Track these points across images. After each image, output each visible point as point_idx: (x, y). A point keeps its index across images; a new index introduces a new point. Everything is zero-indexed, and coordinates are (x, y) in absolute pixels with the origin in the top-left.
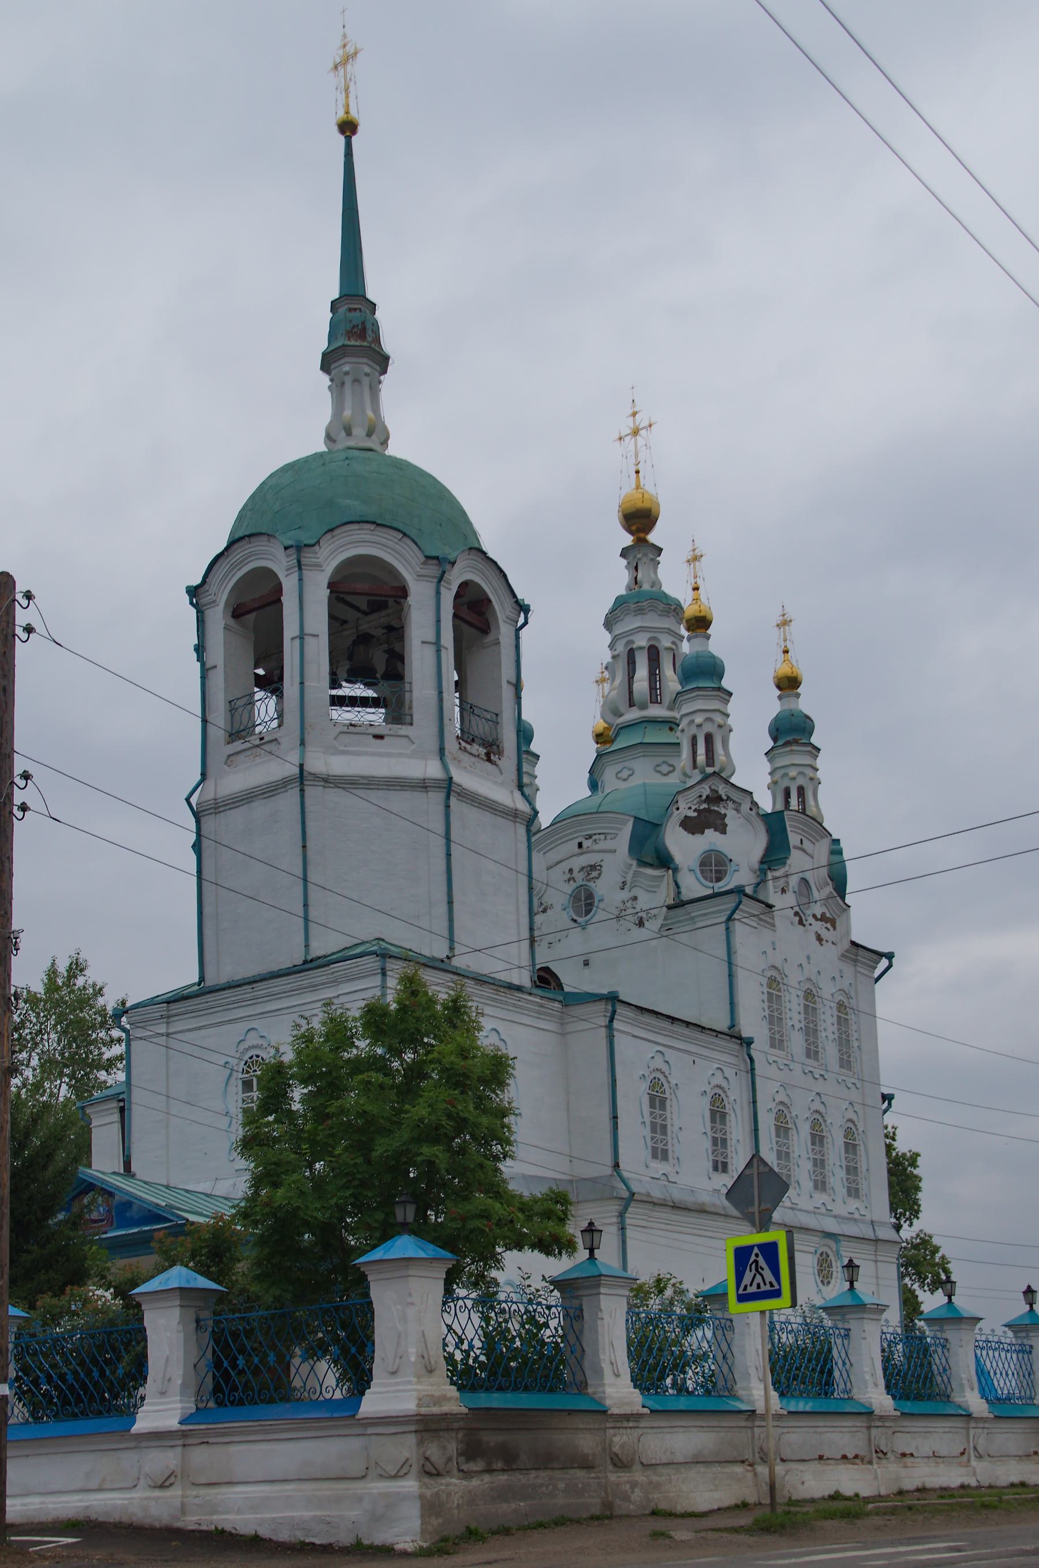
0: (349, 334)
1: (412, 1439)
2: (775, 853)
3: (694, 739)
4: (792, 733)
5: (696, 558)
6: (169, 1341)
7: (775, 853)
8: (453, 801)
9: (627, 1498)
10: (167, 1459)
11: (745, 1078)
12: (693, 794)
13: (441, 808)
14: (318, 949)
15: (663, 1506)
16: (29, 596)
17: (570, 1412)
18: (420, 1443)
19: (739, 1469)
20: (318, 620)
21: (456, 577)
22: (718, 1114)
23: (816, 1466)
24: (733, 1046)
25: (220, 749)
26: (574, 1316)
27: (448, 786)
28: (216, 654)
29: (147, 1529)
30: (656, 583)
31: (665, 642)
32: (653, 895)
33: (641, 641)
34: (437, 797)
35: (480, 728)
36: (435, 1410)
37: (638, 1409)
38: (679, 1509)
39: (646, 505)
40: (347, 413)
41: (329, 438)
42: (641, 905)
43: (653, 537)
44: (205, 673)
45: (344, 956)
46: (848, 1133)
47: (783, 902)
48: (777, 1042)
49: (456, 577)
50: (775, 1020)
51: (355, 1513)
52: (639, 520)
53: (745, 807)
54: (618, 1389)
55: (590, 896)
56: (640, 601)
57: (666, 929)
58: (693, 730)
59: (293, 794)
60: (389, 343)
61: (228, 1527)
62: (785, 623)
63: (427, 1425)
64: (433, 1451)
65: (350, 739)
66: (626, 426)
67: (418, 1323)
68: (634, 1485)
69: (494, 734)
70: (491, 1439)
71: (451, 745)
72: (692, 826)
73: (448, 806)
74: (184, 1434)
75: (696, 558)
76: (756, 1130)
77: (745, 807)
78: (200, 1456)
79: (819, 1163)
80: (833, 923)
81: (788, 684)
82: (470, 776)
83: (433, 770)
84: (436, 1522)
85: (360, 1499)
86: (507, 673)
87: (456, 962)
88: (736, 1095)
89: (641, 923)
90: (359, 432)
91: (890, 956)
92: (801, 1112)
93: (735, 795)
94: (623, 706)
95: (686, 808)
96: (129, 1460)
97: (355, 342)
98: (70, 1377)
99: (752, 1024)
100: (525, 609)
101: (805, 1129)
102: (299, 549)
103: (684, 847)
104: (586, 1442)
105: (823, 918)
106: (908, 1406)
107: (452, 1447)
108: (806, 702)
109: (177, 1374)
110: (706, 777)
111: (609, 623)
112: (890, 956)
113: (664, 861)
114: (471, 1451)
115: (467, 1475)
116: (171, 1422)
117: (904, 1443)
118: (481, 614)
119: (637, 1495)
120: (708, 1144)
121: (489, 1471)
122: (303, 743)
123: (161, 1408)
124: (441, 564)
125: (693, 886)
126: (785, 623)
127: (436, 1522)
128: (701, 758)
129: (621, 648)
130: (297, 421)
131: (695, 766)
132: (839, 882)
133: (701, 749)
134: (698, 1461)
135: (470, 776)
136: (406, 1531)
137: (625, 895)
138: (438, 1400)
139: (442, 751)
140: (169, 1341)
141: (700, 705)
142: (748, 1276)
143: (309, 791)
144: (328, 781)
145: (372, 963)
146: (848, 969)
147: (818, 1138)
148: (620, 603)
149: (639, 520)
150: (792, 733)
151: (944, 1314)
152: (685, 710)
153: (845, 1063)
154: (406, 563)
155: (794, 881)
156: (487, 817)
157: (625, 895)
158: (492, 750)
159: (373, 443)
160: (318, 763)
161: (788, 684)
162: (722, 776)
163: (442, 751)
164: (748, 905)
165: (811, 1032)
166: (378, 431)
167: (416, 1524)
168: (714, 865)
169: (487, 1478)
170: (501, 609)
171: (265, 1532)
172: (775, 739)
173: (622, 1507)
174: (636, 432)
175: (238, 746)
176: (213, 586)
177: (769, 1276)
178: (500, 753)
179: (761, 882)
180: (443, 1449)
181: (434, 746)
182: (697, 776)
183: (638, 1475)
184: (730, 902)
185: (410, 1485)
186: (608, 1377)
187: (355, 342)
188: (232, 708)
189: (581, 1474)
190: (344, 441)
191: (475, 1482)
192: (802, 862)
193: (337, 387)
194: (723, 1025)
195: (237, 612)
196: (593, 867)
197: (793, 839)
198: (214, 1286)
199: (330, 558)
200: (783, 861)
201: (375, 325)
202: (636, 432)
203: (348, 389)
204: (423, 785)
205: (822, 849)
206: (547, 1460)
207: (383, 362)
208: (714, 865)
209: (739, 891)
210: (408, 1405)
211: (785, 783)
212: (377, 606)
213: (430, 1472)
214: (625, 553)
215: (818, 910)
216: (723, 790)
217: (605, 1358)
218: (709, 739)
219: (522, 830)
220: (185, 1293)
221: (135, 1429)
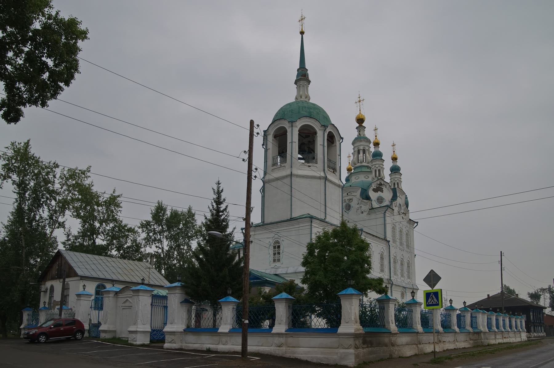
0: (302, 76)
1: (352, 339)
2: (394, 198)
3: (376, 170)
4: (395, 170)
5: (376, 129)
6: (281, 311)
7: (394, 198)
8: (327, 182)
9: (394, 354)
10: (282, 340)
11: (388, 250)
12: (375, 183)
13: (324, 184)
14: (294, 216)
15: (401, 355)
16: (258, 126)
17: (384, 333)
18: (355, 340)
19: (415, 346)
20: (296, 138)
21: (328, 130)
22: (382, 258)
23: (428, 345)
24: (385, 242)
25: (270, 168)
26: (382, 309)
27: (326, 178)
28: (270, 145)
29: (332, 366)
30: (364, 135)
31: (367, 148)
32: (365, 207)
33: (362, 148)
34: (323, 181)
35: (332, 165)
36: (358, 332)
37: (397, 332)
38: (404, 356)
39: (362, 117)
40: (301, 93)
41: (296, 98)
42: (362, 208)
43: (363, 125)
44: (266, 151)
45: (300, 218)
46: (408, 264)
47: (396, 209)
48: (394, 241)
49: (328, 130)
50: (394, 236)
51: (335, 357)
52: (360, 121)
53: (388, 186)
54: (393, 327)
55: (350, 206)
56: (361, 139)
57: (369, 214)
58: (376, 168)
59: (289, 179)
60: (310, 78)
61: (298, 358)
62: (394, 145)
63: (356, 336)
64: (357, 342)
65: (300, 168)
66: (357, 100)
67: (351, 309)
68: (396, 350)
69: (333, 167)
70: (368, 339)
71: (326, 169)
72: (375, 190)
73: (325, 183)
74: (286, 334)
75: (376, 129)
76: (390, 262)
77: (388, 186)
78: (290, 340)
79: (402, 270)
80: (405, 214)
81: (394, 159)
82: (331, 176)
83: (322, 174)
84: (358, 360)
85: (337, 353)
86: (338, 153)
87: (326, 220)
88: (386, 254)
89: (362, 213)
90: (303, 97)
91: (417, 223)
92: (399, 258)
93: (385, 184)
94: (356, 162)
95: (374, 186)
96: (270, 339)
97: (303, 77)
98: (252, 318)
99: (389, 237)
100: (342, 138)
101: (399, 262)
102: (292, 123)
103: (373, 195)
104: (386, 340)
105: (404, 213)
106: (426, 330)
107: (361, 341)
108: (399, 163)
109: (284, 319)
110: (378, 179)
111: (353, 144)
112: (417, 223)
113: (368, 198)
114: (364, 343)
115: (363, 348)
116: (283, 331)
117: (444, 339)
118: (332, 139)
119: (396, 353)
120: (380, 265)
121: (368, 347)
122: (291, 167)
123: (280, 327)
124: (325, 127)
125: (375, 205)
126: (394, 145)
127: (358, 360)
128: (377, 175)
129: (356, 149)
130: (289, 95)
131: (376, 176)
132: (407, 205)
133: (377, 173)
134: (407, 344)
135: (331, 176)
136: (351, 361)
137: (358, 206)
138: (358, 330)
139: (324, 170)
140: (281, 311)
141: (377, 163)
142: (430, 300)
143: (293, 178)
144: (298, 176)
145: (308, 219)
146: (408, 225)
147: (402, 264)
148: (356, 139)
149: (360, 121)
150: (395, 170)
151: (449, 308)
152: (374, 164)
153: (408, 246)
154: (316, 126)
155: (398, 204)
156: (334, 186)
157: (358, 206)
158: (334, 170)
159: (306, 100)
160: (295, 172)
161: (394, 159)
162: (382, 179)
163: (324, 170)
164: (389, 210)
165: (401, 239)
166: (307, 97)
167: (353, 360)
168: (380, 200)
169: (367, 349)
170: (337, 138)
171: (309, 360)
172: (391, 172)
173: (394, 356)
174: (360, 101)
175: (275, 167)
176: (270, 130)
177: (435, 300)
178: (336, 171)
179: (392, 204)
180: (359, 342)
181: (322, 169)
182: (376, 179)
183: (396, 348)
184: (385, 209)
185: (352, 351)
186: (391, 324)
187: (303, 77)
188: (273, 159)
189: (385, 348)
190: (299, 99)
191: (365, 350)
192: (400, 200)
193: (298, 88)
194: (383, 237)
195: (275, 137)
196: (350, 199)
197: (398, 194)
198: (290, 297)
199: (299, 124)
200: (396, 200)
201: (308, 74)
202: (360, 101)
203: (301, 88)
204: (320, 178)
205: (404, 197)
206: (379, 344)
207: (309, 82)
208: (380, 200)
209: (387, 206)
210: (352, 331)
211: (394, 182)
212: (307, 136)
213: (356, 348)
214: (357, 128)
215: (403, 211)
216: (382, 183)
217: (390, 319)
218: (379, 170)
219: (341, 190)
220: (287, 299)
221: (272, 332)
